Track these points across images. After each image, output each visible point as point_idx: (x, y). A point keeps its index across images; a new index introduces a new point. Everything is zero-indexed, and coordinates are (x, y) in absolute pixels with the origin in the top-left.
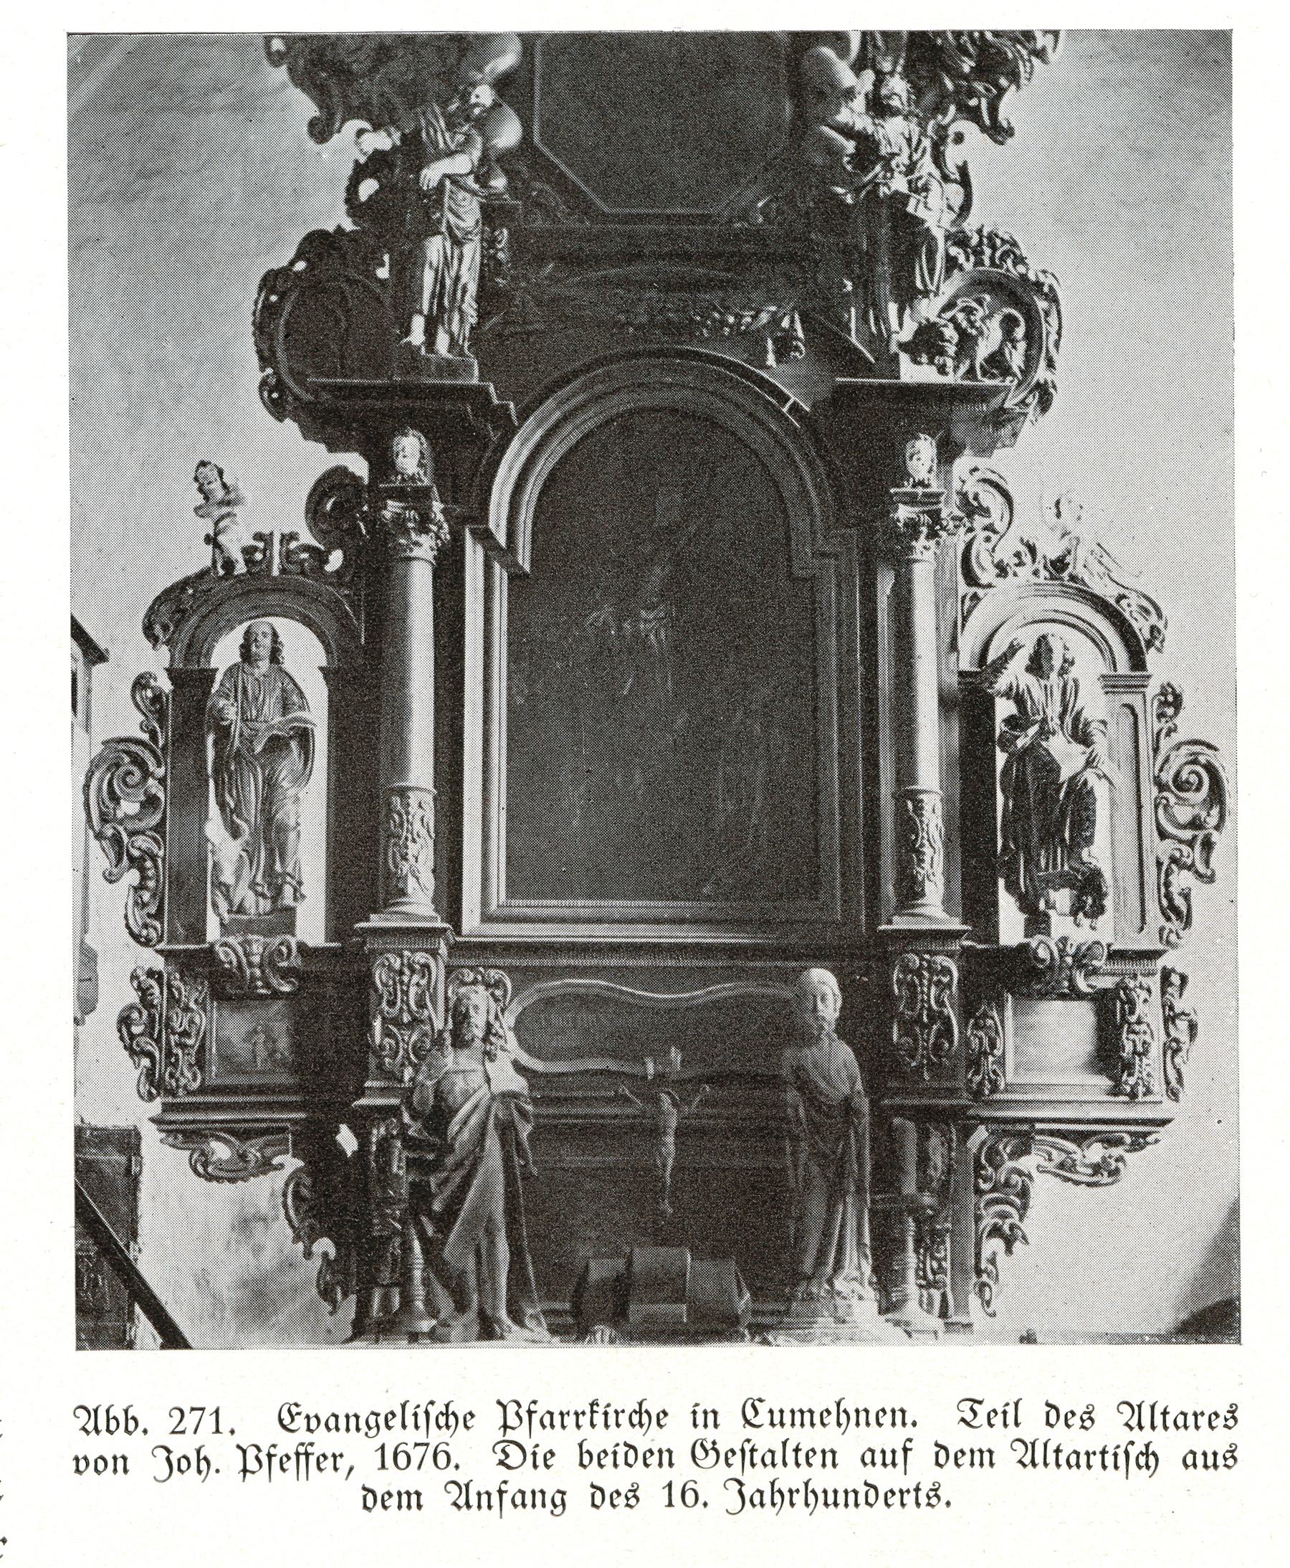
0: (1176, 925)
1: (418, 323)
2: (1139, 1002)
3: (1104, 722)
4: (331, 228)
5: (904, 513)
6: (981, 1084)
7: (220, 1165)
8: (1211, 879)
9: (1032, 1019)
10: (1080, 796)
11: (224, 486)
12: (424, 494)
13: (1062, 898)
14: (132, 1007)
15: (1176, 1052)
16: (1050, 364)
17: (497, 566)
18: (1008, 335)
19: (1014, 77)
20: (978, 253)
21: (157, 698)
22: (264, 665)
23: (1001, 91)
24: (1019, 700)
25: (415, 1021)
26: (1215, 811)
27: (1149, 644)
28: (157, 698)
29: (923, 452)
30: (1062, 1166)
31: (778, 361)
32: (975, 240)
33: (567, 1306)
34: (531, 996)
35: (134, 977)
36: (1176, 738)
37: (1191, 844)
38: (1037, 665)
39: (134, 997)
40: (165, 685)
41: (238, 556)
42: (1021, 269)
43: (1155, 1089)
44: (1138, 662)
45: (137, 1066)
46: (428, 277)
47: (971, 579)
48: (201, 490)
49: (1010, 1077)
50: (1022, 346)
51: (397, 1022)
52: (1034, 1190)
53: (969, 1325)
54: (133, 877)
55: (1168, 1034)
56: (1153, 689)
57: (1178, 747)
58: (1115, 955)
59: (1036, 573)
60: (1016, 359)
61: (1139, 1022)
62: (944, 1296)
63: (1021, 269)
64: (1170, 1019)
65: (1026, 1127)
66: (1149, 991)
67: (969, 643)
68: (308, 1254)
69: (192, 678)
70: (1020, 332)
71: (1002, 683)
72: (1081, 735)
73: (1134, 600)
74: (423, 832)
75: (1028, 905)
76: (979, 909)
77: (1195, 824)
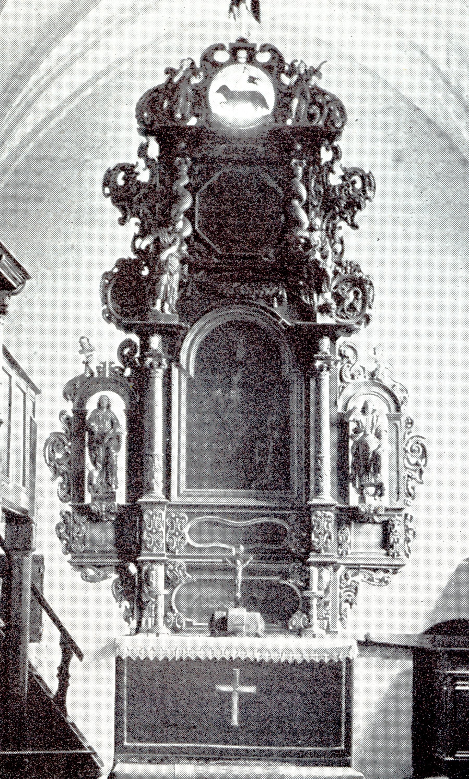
0: (409, 499)
1: (159, 302)
2: (396, 526)
3: (386, 431)
4: (126, 258)
5: (318, 364)
6: (342, 552)
7: (92, 577)
8: (422, 483)
9: (360, 530)
10: (376, 458)
11: (90, 345)
12: (160, 356)
13: (371, 490)
14: (61, 523)
15: (408, 541)
16: (370, 307)
17: (183, 376)
18: (356, 298)
19: (359, 207)
20: (346, 268)
21: (68, 419)
22: (105, 410)
23: (354, 212)
24: (358, 423)
25: (157, 532)
26: (424, 460)
27: (402, 403)
28: (68, 419)
29: (326, 343)
30: (368, 579)
31: (279, 305)
32: (345, 264)
33: (207, 624)
34: (194, 522)
35: (61, 513)
36: (411, 435)
37: (415, 471)
38: (364, 411)
39: (61, 520)
40: (71, 415)
41: (95, 371)
42: (361, 274)
43: (400, 554)
44: (398, 409)
45: (62, 543)
46: (163, 288)
47: (342, 380)
48: (81, 346)
49: (353, 549)
50: (360, 301)
51: (151, 532)
52: (360, 587)
53: (336, 632)
54: (60, 479)
55: (406, 535)
56: (403, 418)
57: (412, 438)
58: (387, 510)
59: (365, 377)
60: (359, 306)
61: (396, 531)
62: (328, 622)
63: (361, 274)
64: (407, 531)
65: (357, 567)
66: (400, 521)
67: (340, 403)
68: (120, 606)
69: (80, 413)
70: (360, 296)
71: (351, 418)
72: (378, 436)
73: (398, 387)
74: (159, 469)
75: (361, 490)
76: (343, 493)
77: (417, 464)
